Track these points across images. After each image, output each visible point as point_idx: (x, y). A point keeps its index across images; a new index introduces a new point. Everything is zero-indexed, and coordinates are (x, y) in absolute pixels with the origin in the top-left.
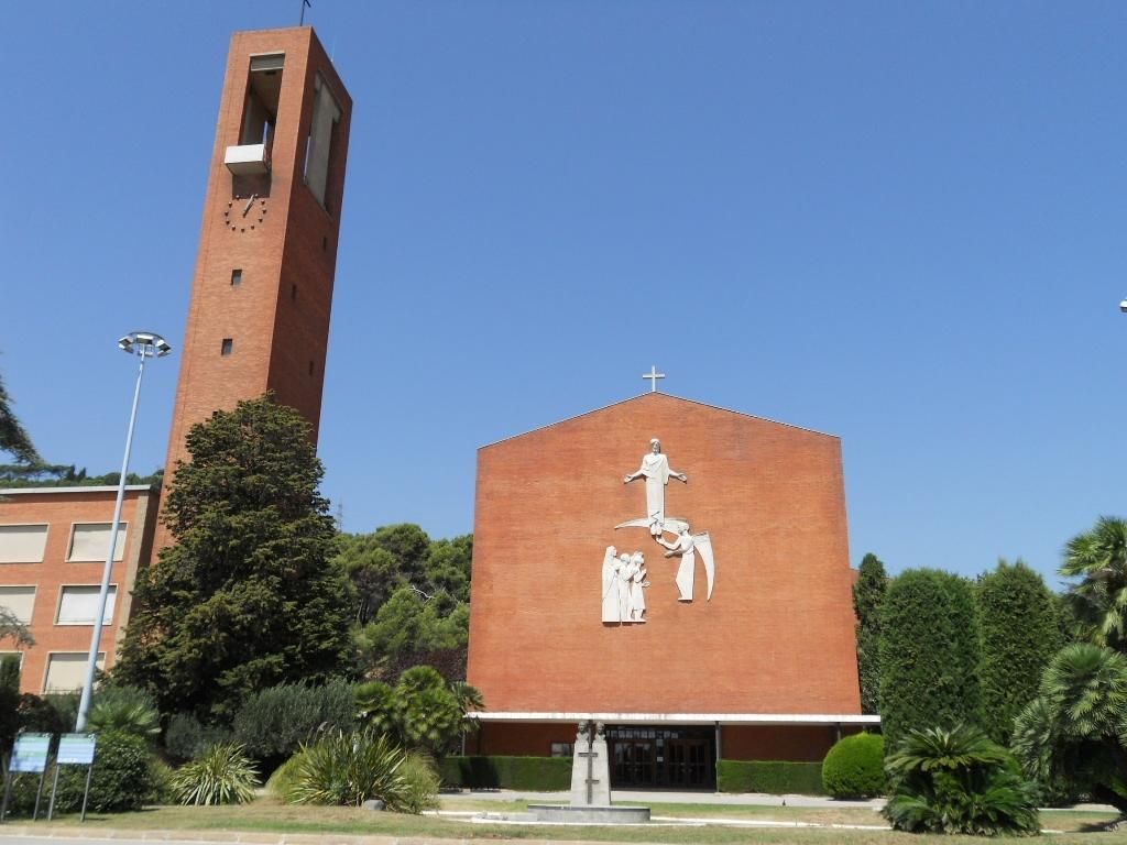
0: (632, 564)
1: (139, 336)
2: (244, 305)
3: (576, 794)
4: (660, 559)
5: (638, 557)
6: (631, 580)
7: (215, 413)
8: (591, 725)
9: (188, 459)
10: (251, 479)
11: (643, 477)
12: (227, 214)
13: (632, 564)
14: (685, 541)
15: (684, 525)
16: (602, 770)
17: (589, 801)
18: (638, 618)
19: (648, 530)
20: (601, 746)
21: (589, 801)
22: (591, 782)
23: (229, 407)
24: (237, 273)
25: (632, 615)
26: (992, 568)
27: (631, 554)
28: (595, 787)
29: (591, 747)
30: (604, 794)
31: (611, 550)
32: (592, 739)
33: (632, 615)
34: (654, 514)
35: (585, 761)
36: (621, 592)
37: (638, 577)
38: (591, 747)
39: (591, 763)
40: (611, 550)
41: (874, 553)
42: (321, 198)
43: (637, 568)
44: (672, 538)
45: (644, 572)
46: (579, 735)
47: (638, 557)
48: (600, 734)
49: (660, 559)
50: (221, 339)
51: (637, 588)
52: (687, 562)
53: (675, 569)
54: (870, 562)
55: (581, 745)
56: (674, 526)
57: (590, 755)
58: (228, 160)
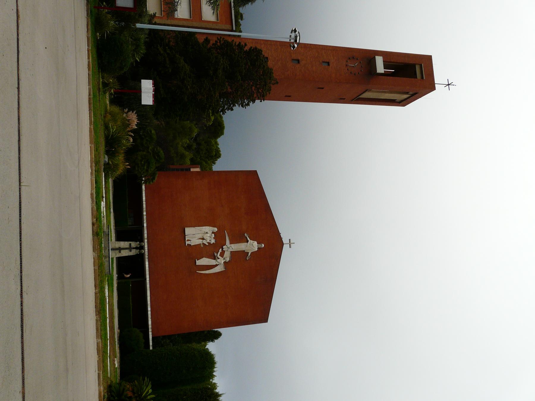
0: (210, 239)
1: (298, 37)
2: (314, 68)
3: (114, 243)
4: (211, 250)
5: (213, 241)
6: (203, 239)
7: (267, 58)
8: (142, 248)
9: (246, 48)
10: (239, 77)
11: (247, 241)
12: (353, 58)
13: (210, 239)
14: (221, 261)
15: (228, 260)
16: (125, 253)
17: (112, 249)
18: (187, 243)
19: (225, 244)
20: (134, 252)
21: (112, 249)
22: (120, 249)
23: (270, 64)
24: (328, 64)
25: (188, 240)
26: (212, 353)
27: (214, 238)
28: (117, 251)
29: (134, 248)
30: (114, 255)
31: (216, 229)
32: (136, 248)
33: (188, 240)
34: (230, 247)
35: (128, 246)
36: (198, 235)
37: (204, 242)
38: (134, 248)
39: (126, 249)
40: (216, 229)
41: (221, 337)
42: (362, 96)
43: (208, 241)
44: (222, 255)
45: (207, 244)
46: (138, 243)
47: (213, 241)
48: (139, 244)
49: (211, 250)
50: (299, 58)
51: (200, 242)
52: (212, 262)
53: (209, 257)
54: (217, 335)
55: (134, 244)
56: (227, 255)
57: (130, 248)
58: (377, 57)
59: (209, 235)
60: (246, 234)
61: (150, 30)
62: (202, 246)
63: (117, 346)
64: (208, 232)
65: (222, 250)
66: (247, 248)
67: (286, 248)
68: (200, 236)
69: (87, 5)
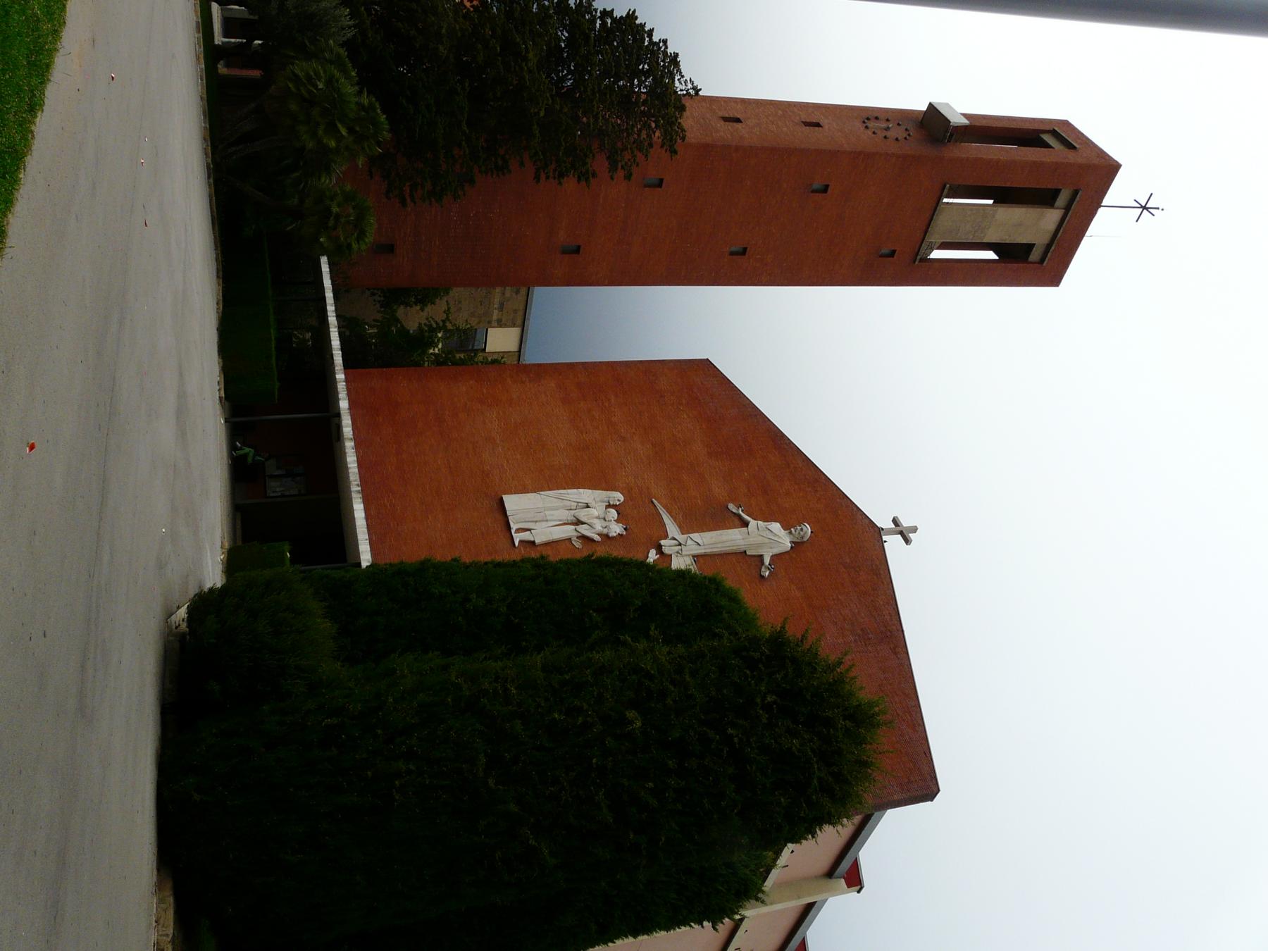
6: (578, 522)
11: (746, 524)
18: (518, 538)
31: (618, 497)
37: (584, 530)
40: (618, 497)
45: (597, 538)
47: (616, 529)
51: (568, 531)
59: (595, 512)
60: (732, 507)
61: (347, 365)
62: (578, 544)
63: (239, 527)
64: (592, 503)
65: (331, 62)
66: (751, 540)
67: (893, 545)
68: (567, 515)
69: (48, 66)
